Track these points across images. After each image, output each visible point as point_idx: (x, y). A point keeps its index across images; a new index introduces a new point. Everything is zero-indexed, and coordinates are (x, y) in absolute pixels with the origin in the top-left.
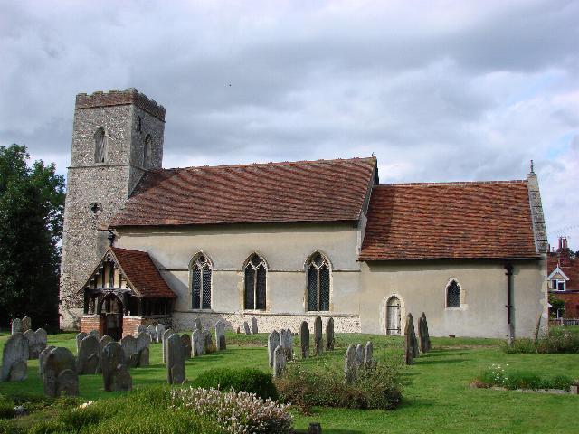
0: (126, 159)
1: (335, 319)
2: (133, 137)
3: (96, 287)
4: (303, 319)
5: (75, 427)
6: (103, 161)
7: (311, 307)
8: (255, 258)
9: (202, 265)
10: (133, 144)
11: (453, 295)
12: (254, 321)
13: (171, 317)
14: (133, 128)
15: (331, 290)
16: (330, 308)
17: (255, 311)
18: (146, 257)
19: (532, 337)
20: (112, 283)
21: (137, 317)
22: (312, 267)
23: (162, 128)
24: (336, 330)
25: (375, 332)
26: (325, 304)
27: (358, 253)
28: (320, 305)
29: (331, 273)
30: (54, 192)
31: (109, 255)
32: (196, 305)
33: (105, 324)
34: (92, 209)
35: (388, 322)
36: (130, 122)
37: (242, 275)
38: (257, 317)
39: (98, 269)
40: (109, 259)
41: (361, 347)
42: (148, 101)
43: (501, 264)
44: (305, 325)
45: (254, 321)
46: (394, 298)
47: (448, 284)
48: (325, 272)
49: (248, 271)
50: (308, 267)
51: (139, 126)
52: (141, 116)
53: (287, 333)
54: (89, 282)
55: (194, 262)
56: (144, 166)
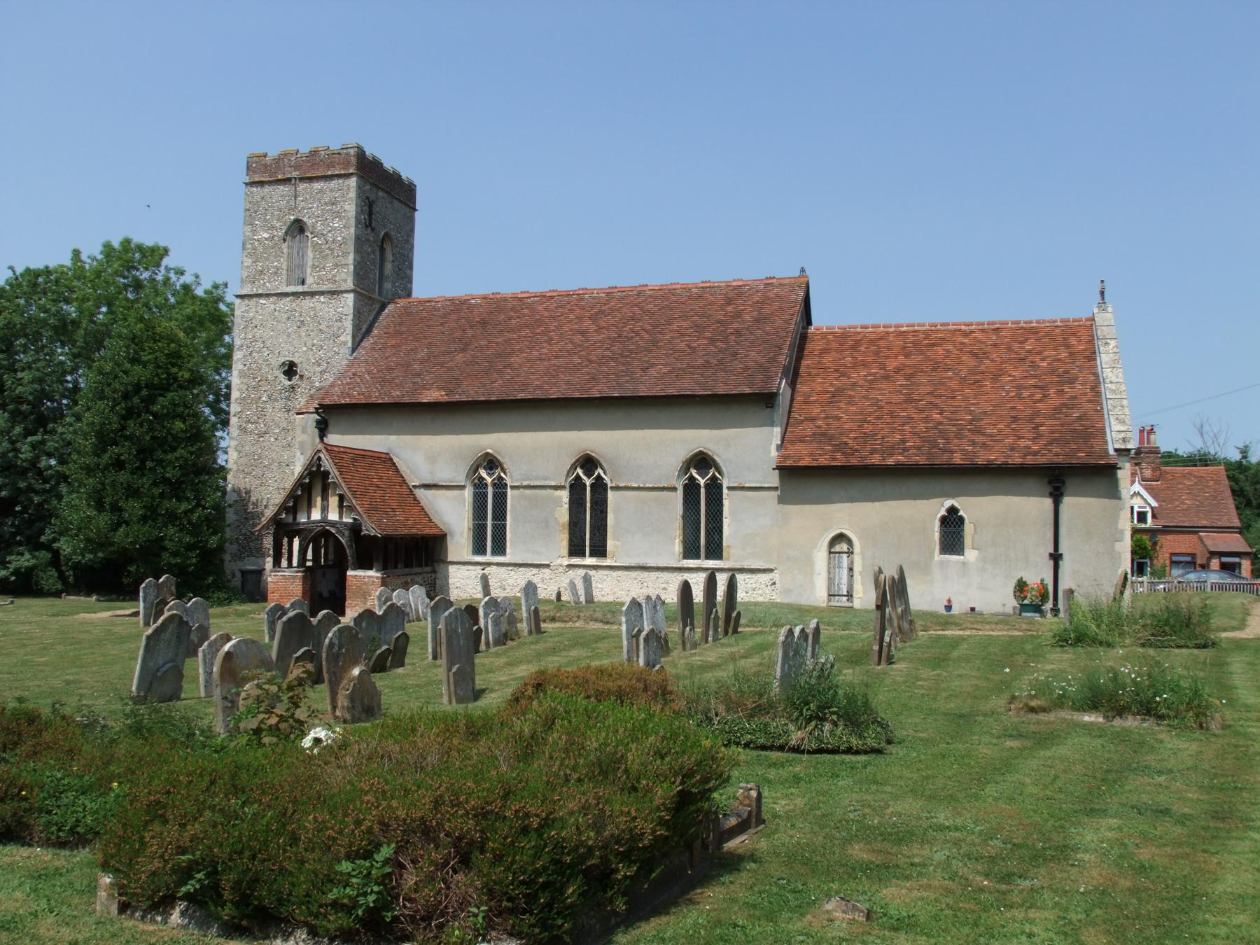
0: (346, 279)
1: (739, 577)
2: (358, 238)
3: (295, 518)
4: (678, 579)
5: (399, 895)
6: (303, 283)
7: (691, 551)
8: (588, 463)
9: (490, 475)
10: (358, 250)
11: (952, 525)
12: (587, 581)
13: (434, 572)
14: (358, 221)
15: (726, 522)
16: (725, 554)
17: (589, 561)
18: (386, 461)
19: (67, 262)
20: (325, 509)
21: (371, 573)
22: (692, 479)
23: (412, 220)
24: (741, 596)
25: (804, 600)
26: (715, 550)
27: (774, 453)
28: (707, 548)
29: (725, 491)
30: (104, 305)
31: (319, 459)
32: (479, 548)
33: (313, 586)
34: (285, 373)
35: (831, 581)
36: (350, 208)
37: (564, 495)
38: (592, 573)
39: (299, 483)
40: (319, 466)
41: (803, 630)
42: (385, 171)
43: (1030, 483)
44: (686, 589)
45: (587, 581)
46: (840, 538)
47: (943, 512)
48: (715, 489)
49: (576, 488)
50: (684, 480)
51: (368, 210)
52: (372, 197)
53: (656, 603)
54: (283, 507)
55: (476, 470)
56: (380, 293)
